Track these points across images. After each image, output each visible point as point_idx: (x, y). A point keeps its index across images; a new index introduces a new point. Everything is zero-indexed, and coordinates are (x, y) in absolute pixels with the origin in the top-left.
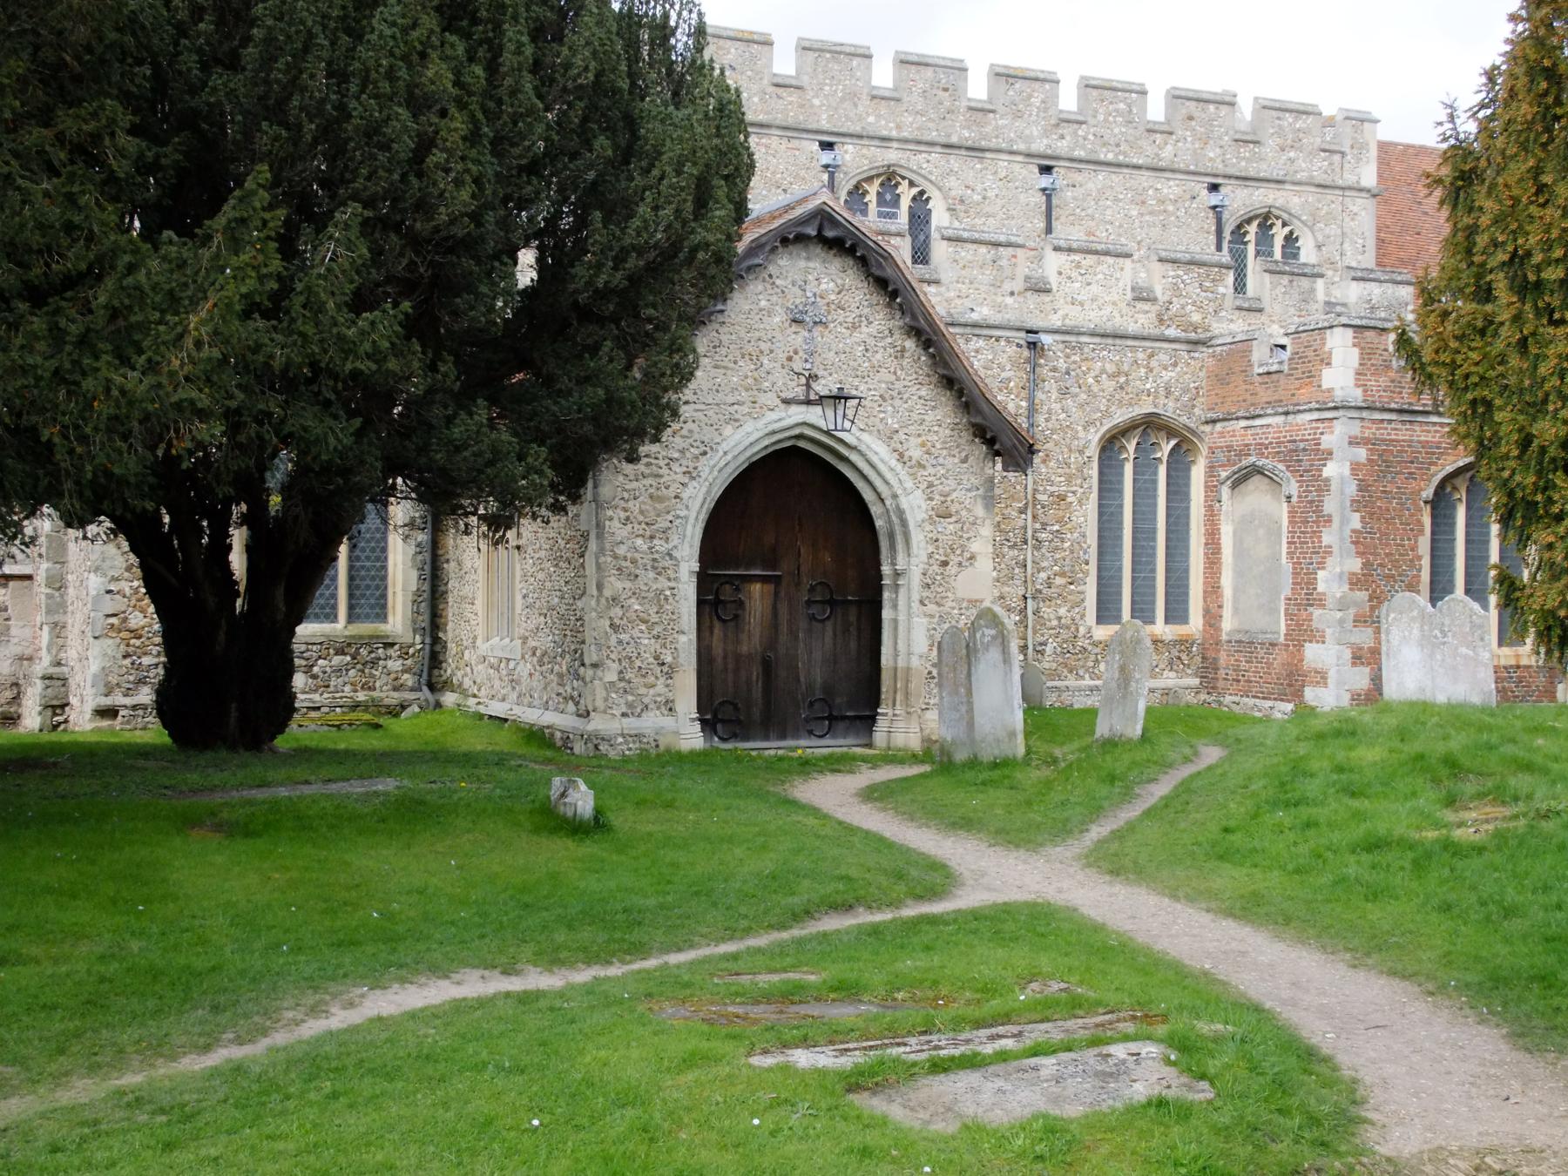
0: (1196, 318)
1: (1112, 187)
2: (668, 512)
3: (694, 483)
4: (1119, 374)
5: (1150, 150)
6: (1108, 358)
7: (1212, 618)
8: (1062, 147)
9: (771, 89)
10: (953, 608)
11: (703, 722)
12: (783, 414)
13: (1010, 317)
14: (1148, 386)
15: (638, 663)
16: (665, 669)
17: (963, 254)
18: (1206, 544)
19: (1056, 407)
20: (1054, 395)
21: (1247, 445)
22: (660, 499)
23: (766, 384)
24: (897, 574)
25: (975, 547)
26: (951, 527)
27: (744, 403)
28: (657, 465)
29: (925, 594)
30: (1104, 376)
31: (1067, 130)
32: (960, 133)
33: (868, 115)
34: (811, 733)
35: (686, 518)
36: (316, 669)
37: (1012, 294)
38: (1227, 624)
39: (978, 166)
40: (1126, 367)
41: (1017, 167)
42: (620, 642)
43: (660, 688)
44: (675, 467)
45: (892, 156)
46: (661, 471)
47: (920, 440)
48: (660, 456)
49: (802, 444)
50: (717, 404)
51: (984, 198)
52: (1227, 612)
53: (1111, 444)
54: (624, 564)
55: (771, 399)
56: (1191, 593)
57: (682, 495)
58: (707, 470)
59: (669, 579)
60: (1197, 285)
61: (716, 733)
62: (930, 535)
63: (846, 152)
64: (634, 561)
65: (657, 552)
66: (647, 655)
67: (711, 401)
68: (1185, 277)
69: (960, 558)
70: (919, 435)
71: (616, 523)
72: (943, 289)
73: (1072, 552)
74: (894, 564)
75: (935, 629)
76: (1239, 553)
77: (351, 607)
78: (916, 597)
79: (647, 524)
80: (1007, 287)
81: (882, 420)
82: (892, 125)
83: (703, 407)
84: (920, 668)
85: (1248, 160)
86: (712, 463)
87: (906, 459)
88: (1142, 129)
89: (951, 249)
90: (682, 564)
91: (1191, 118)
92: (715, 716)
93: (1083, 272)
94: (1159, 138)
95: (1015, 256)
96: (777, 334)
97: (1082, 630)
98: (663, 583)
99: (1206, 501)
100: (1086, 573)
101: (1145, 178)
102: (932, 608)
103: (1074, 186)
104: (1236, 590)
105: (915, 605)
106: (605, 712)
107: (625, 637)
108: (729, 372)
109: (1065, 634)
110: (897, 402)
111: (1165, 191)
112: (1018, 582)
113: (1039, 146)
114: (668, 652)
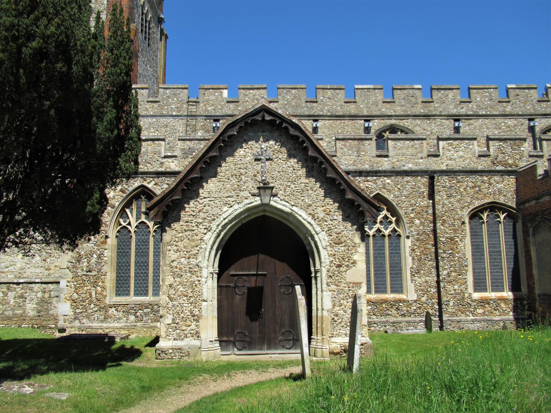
0: (510, 162)
1: (486, 124)
2: (197, 246)
3: (210, 233)
4: (475, 187)
5: (501, 109)
6: (469, 181)
7: (531, 288)
8: (463, 111)
9: (344, 104)
10: (345, 287)
11: (221, 342)
12: (253, 200)
13: (423, 167)
14: (490, 191)
15: (182, 315)
16: (196, 318)
17: (399, 144)
18: (526, 256)
19: (446, 202)
20: (445, 197)
21: (537, 211)
22: (193, 241)
23: (244, 187)
24: (316, 272)
25: (356, 257)
26: (342, 248)
27: (233, 196)
28: (191, 226)
29: (329, 281)
30: (468, 188)
31: (463, 105)
32: (420, 109)
33: (383, 108)
34: (283, 347)
35: (206, 249)
36: (138, 314)
37: (422, 158)
38: (537, 292)
39: (428, 122)
40: (479, 183)
41: (444, 121)
42: (173, 306)
43: (193, 326)
44: (201, 227)
45: (393, 122)
46: (193, 228)
47: (323, 209)
48: (193, 222)
49: (267, 214)
50: (220, 198)
51: (431, 133)
52: (536, 286)
53: (475, 215)
54: (176, 270)
55: (246, 194)
56: (521, 278)
57: (204, 238)
58: (215, 227)
59: (198, 277)
60: (510, 148)
61: (235, 347)
62: (331, 252)
63: (374, 122)
64: (180, 269)
65: (191, 264)
66: (187, 311)
67: (216, 196)
68: (503, 145)
69: (348, 263)
70: (323, 206)
71: (172, 252)
72: (390, 159)
73: (459, 261)
74: (315, 267)
75: (335, 297)
76: (539, 258)
77: (135, 291)
78: (324, 282)
79: (187, 252)
80: (420, 155)
81: (303, 200)
82: (392, 111)
83: (214, 199)
84: (328, 316)
85: (546, 108)
86: (217, 223)
87: (316, 217)
88: (497, 101)
89: (393, 143)
90: (203, 269)
91: (517, 95)
92: (235, 338)
93: (454, 147)
94: (504, 104)
95: (422, 143)
96: (249, 166)
97: (466, 295)
98: (194, 278)
99: (523, 238)
100: (467, 271)
101: (499, 120)
102: (333, 287)
103: (469, 125)
104: (539, 275)
105: (325, 286)
106: (165, 338)
107: (176, 303)
108: (225, 183)
109: (458, 297)
110: (310, 192)
111: (509, 123)
112: (434, 275)
113: (454, 111)
114: (197, 310)
